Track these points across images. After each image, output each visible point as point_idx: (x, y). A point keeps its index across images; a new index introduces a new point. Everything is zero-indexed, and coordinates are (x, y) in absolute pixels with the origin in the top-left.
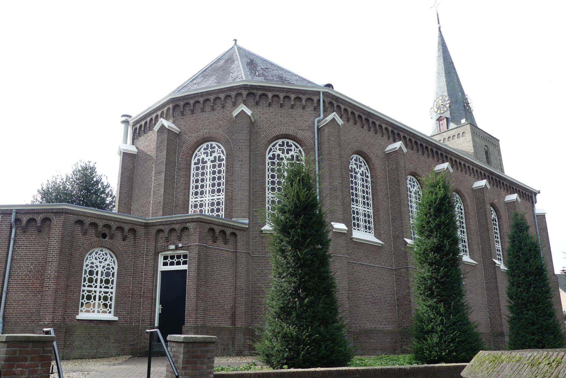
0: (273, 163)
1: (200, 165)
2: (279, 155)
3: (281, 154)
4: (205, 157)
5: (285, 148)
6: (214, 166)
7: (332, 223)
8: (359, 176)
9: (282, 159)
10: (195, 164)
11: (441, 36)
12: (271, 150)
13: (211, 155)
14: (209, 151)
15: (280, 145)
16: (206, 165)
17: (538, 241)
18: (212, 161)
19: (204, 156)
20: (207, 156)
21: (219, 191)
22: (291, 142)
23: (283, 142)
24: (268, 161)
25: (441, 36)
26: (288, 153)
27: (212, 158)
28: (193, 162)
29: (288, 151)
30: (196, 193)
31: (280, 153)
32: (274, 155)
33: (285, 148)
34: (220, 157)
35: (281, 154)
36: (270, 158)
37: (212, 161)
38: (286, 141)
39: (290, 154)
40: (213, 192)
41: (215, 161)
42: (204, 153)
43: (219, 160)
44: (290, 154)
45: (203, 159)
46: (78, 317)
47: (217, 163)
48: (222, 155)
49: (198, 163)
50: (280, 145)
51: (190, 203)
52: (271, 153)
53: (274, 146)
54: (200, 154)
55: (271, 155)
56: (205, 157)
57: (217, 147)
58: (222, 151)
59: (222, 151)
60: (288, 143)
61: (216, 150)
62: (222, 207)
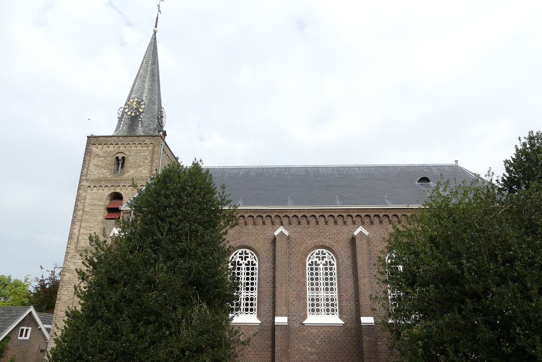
0: (312, 269)
3: (317, 261)
4: (240, 261)
5: (321, 256)
6: (248, 269)
7: (341, 322)
8: (321, 266)
9: (319, 265)
11: (154, 39)
12: (310, 258)
13: (245, 260)
14: (244, 256)
15: (317, 254)
16: (319, 267)
18: (324, 265)
20: (242, 260)
22: (325, 251)
23: (319, 251)
24: (307, 266)
25: (154, 39)
26: (249, 262)
27: (246, 262)
29: (323, 258)
31: (317, 260)
32: (312, 262)
35: (317, 261)
36: (309, 265)
37: (324, 265)
38: (244, 250)
39: (325, 261)
41: (248, 265)
42: (240, 257)
43: (252, 265)
44: (325, 261)
45: (238, 262)
46: (307, 321)
48: (332, 260)
49: (312, 265)
50: (240, 254)
52: (310, 260)
53: (312, 255)
54: (311, 258)
55: (310, 262)
56: (240, 261)
57: (250, 254)
58: (332, 257)
60: (322, 251)
61: (249, 256)
62: (255, 302)
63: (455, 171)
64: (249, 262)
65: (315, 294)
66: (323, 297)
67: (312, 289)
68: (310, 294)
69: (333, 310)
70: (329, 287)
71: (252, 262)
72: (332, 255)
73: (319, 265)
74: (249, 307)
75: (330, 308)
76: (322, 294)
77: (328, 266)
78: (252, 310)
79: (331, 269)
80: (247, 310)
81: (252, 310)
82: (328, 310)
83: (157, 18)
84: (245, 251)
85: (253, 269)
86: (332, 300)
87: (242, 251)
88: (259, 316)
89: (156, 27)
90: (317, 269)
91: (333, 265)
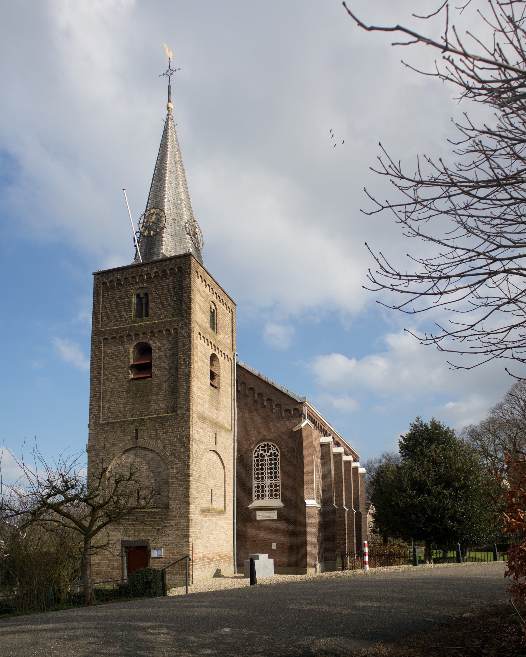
1: (260, 458)
2: (262, 454)
7: (283, 505)
8: (266, 458)
9: (264, 456)
10: (255, 457)
12: (256, 451)
13: (268, 452)
14: (266, 448)
15: (262, 447)
17: (166, 535)
18: (269, 456)
19: (261, 452)
20: (265, 452)
21: (276, 477)
22: (270, 444)
26: (271, 453)
27: (269, 454)
28: (254, 456)
30: (258, 478)
33: (266, 448)
34: (275, 453)
37: (269, 456)
40: (271, 477)
41: (271, 456)
42: (262, 450)
47: (273, 457)
48: (276, 452)
50: (262, 447)
51: (254, 485)
52: (256, 453)
57: (272, 446)
58: (277, 449)
59: (277, 449)
61: (271, 448)
63: (89, 425)
64: (271, 453)
65: (260, 482)
66: (267, 485)
67: (258, 478)
68: (256, 483)
69: (276, 495)
70: (273, 475)
71: (275, 453)
72: (277, 447)
73: (264, 456)
74: (274, 493)
75: (274, 493)
76: (267, 482)
77: (273, 457)
78: (263, 496)
79: (275, 459)
80: (271, 495)
81: (276, 495)
82: (271, 495)
83: (349, 12)
84: (268, 444)
85: (275, 459)
86: (276, 486)
87: (265, 445)
88: (283, 501)
89: (169, 101)
90: (262, 460)
91: (277, 455)
